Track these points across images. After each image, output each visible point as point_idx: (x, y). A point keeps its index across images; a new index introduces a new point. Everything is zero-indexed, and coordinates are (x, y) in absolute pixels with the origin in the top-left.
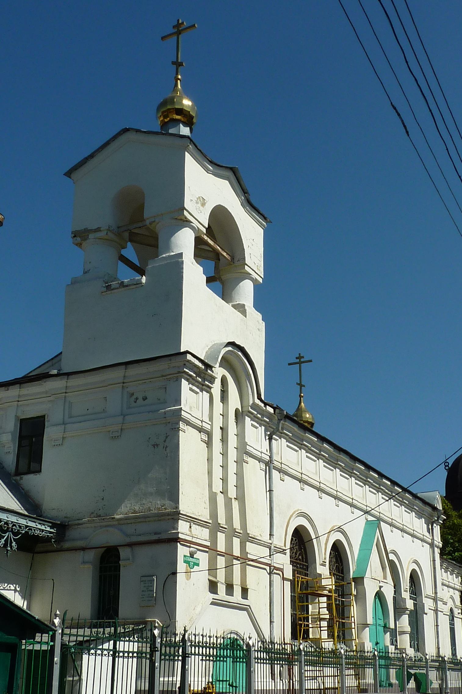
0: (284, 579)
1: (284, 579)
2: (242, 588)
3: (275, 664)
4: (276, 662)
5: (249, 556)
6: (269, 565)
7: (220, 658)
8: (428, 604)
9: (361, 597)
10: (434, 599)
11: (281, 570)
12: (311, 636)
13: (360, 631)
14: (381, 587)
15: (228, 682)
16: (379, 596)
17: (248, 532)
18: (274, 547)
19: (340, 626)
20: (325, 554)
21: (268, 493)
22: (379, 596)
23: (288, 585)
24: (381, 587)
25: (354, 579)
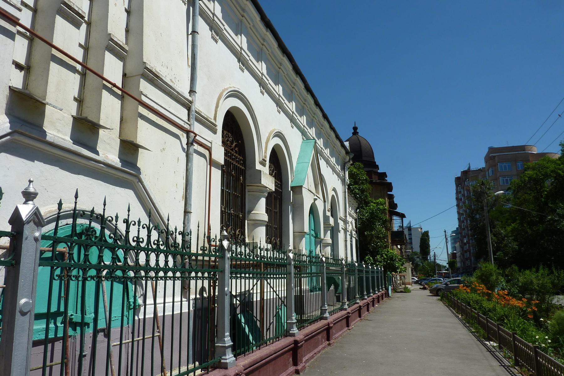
0: (212, 163)
1: (212, 163)
2: (121, 140)
3: (190, 278)
4: (193, 274)
5: (144, 99)
6: (188, 132)
7: (166, 273)
8: (341, 223)
9: (298, 207)
10: (344, 222)
11: (209, 149)
12: (247, 241)
13: (297, 239)
14: (315, 200)
15: (59, 319)
16: (313, 210)
17: (145, 60)
18: (196, 112)
19: (276, 233)
20: (266, 152)
21: (190, 37)
22: (313, 210)
23: (217, 174)
24: (315, 200)
25: (292, 188)
